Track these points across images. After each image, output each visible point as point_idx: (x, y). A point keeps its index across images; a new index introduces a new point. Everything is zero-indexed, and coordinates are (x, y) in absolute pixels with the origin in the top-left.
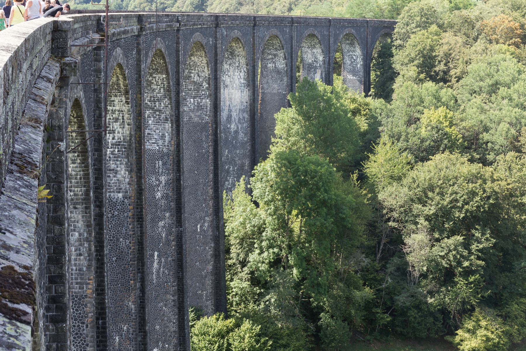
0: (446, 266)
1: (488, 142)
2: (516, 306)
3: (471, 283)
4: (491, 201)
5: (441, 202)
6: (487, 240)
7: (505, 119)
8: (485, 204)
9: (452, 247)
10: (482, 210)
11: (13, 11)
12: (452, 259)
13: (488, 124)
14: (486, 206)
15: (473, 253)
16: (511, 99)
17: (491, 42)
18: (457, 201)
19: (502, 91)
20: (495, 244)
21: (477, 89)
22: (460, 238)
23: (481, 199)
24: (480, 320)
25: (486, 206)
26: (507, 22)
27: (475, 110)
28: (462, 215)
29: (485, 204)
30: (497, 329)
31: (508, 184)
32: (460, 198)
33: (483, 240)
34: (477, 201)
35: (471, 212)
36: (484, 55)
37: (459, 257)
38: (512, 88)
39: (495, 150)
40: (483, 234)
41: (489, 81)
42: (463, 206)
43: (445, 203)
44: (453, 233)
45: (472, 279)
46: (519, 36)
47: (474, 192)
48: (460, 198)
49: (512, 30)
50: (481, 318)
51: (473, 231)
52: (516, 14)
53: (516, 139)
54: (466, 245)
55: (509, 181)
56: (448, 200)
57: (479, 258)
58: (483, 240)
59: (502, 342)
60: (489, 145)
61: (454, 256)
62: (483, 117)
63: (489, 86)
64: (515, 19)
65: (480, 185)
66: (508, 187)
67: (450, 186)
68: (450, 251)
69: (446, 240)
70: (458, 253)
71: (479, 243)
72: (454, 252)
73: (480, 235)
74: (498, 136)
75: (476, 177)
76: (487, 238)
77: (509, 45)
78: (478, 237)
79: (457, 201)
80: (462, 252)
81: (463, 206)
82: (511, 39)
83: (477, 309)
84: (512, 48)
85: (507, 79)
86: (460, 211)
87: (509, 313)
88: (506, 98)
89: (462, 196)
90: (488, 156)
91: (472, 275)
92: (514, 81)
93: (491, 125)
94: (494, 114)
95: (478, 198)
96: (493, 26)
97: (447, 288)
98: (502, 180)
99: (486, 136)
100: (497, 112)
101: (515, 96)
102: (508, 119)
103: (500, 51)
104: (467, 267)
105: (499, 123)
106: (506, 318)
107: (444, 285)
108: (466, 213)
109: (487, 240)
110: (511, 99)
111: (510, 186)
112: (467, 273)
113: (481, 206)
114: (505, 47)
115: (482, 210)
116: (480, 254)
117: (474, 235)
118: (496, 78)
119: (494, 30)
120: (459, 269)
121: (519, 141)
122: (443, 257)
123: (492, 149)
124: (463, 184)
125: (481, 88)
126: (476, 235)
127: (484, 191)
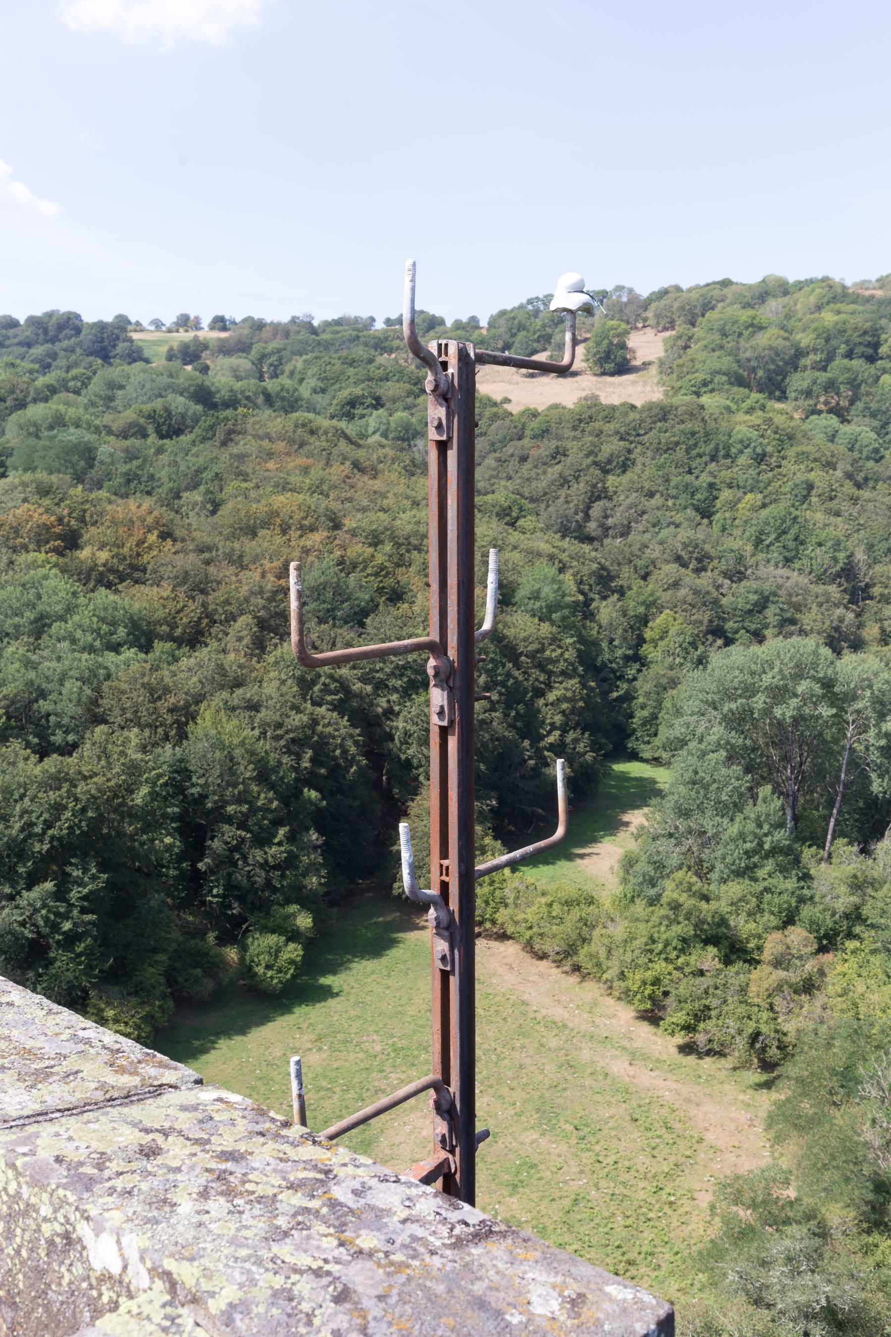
0: (30, 936)
1: (49, 715)
2: (151, 970)
3: (79, 955)
4: (90, 814)
5: (7, 832)
6: (94, 878)
7: (71, 673)
8: (80, 821)
9: (38, 904)
10: (78, 832)
11: (176, 1069)
12: (42, 923)
13: (44, 685)
14: (83, 824)
15: (73, 904)
16: (74, 641)
17: (14, 550)
18: (32, 824)
19: (56, 628)
20: (107, 882)
21: (11, 630)
22: (49, 886)
23: (73, 815)
24: (102, 1010)
25: (83, 824)
26: (36, 515)
27: (17, 665)
28: (46, 847)
29: (80, 821)
30: (133, 1016)
31: (109, 780)
32: (38, 818)
33: (88, 880)
34: (67, 819)
35: (60, 839)
36: (11, 573)
37: (52, 917)
38: (70, 622)
39: (64, 726)
40: (85, 871)
41: (29, 615)
42: (44, 832)
43: (14, 832)
44: (32, 881)
45: (80, 948)
46: (59, 537)
47: (60, 804)
48: (38, 818)
49: (48, 528)
50: (103, 1006)
51: (68, 869)
52: (46, 502)
53: (95, 702)
54: (60, 895)
55: (109, 775)
56: (17, 826)
57: (84, 911)
58: (86, 879)
59: (143, 1034)
60: (52, 719)
61: (46, 919)
62: (32, 675)
63: (31, 623)
64: (47, 511)
65: (68, 791)
66: (109, 784)
67: (16, 801)
68: (36, 911)
69: (25, 894)
70: (49, 911)
71: (79, 886)
72: (44, 912)
73: (80, 873)
74: (65, 703)
75: (58, 779)
76: (93, 875)
77: (47, 553)
78: (78, 877)
79: (32, 824)
80: (57, 907)
81: (44, 832)
82: (47, 542)
83: (92, 993)
84: (53, 558)
85: (59, 608)
86: (41, 841)
87: (141, 982)
88: (64, 639)
89: (41, 816)
90: (52, 738)
91: (80, 942)
92: (70, 609)
93: (49, 686)
94: (50, 666)
95: (68, 814)
96: (14, 524)
97: (37, 971)
98: (96, 775)
99: (44, 706)
100: (54, 664)
101: (79, 634)
102: (74, 673)
103: (34, 565)
104: (70, 930)
105: (61, 682)
106: (140, 992)
107: (29, 967)
108: (50, 842)
109: (94, 878)
110: (74, 641)
111: (112, 783)
112: (71, 939)
113: (75, 825)
114: (41, 557)
115: (78, 832)
116: (85, 903)
117: (70, 875)
118: (40, 607)
119: (16, 531)
120: (58, 937)
121: (98, 706)
122: (23, 924)
123: (59, 725)
124: (40, 795)
125: (17, 627)
126: (75, 874)
127: (76, 800)
